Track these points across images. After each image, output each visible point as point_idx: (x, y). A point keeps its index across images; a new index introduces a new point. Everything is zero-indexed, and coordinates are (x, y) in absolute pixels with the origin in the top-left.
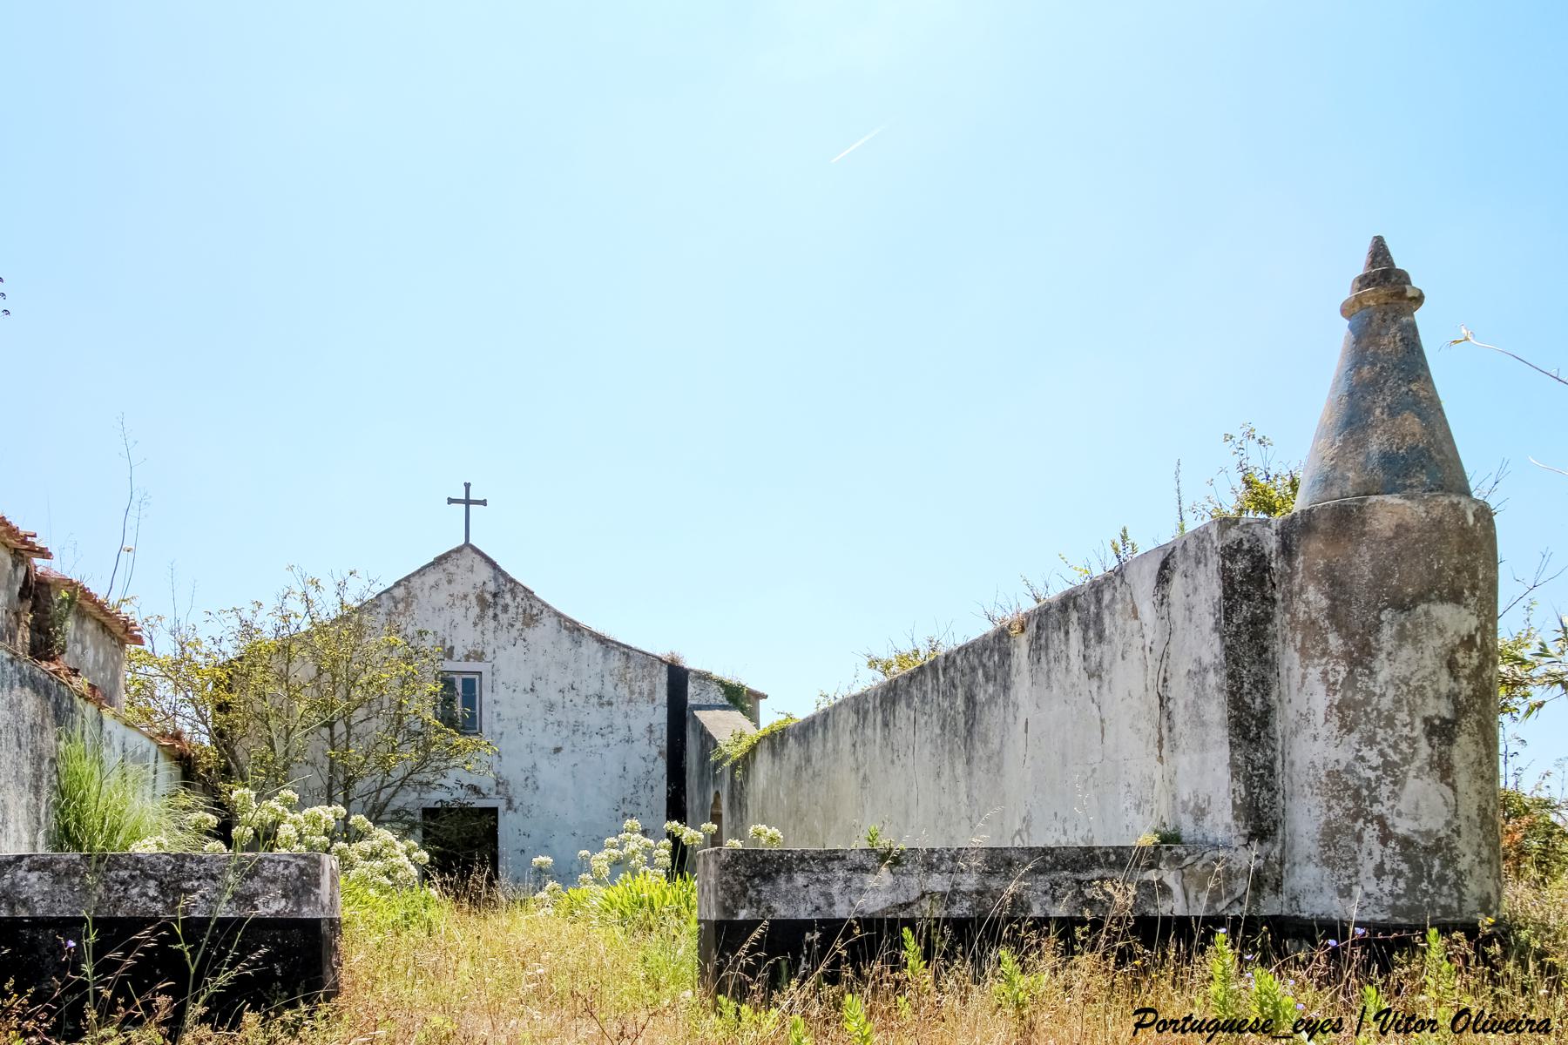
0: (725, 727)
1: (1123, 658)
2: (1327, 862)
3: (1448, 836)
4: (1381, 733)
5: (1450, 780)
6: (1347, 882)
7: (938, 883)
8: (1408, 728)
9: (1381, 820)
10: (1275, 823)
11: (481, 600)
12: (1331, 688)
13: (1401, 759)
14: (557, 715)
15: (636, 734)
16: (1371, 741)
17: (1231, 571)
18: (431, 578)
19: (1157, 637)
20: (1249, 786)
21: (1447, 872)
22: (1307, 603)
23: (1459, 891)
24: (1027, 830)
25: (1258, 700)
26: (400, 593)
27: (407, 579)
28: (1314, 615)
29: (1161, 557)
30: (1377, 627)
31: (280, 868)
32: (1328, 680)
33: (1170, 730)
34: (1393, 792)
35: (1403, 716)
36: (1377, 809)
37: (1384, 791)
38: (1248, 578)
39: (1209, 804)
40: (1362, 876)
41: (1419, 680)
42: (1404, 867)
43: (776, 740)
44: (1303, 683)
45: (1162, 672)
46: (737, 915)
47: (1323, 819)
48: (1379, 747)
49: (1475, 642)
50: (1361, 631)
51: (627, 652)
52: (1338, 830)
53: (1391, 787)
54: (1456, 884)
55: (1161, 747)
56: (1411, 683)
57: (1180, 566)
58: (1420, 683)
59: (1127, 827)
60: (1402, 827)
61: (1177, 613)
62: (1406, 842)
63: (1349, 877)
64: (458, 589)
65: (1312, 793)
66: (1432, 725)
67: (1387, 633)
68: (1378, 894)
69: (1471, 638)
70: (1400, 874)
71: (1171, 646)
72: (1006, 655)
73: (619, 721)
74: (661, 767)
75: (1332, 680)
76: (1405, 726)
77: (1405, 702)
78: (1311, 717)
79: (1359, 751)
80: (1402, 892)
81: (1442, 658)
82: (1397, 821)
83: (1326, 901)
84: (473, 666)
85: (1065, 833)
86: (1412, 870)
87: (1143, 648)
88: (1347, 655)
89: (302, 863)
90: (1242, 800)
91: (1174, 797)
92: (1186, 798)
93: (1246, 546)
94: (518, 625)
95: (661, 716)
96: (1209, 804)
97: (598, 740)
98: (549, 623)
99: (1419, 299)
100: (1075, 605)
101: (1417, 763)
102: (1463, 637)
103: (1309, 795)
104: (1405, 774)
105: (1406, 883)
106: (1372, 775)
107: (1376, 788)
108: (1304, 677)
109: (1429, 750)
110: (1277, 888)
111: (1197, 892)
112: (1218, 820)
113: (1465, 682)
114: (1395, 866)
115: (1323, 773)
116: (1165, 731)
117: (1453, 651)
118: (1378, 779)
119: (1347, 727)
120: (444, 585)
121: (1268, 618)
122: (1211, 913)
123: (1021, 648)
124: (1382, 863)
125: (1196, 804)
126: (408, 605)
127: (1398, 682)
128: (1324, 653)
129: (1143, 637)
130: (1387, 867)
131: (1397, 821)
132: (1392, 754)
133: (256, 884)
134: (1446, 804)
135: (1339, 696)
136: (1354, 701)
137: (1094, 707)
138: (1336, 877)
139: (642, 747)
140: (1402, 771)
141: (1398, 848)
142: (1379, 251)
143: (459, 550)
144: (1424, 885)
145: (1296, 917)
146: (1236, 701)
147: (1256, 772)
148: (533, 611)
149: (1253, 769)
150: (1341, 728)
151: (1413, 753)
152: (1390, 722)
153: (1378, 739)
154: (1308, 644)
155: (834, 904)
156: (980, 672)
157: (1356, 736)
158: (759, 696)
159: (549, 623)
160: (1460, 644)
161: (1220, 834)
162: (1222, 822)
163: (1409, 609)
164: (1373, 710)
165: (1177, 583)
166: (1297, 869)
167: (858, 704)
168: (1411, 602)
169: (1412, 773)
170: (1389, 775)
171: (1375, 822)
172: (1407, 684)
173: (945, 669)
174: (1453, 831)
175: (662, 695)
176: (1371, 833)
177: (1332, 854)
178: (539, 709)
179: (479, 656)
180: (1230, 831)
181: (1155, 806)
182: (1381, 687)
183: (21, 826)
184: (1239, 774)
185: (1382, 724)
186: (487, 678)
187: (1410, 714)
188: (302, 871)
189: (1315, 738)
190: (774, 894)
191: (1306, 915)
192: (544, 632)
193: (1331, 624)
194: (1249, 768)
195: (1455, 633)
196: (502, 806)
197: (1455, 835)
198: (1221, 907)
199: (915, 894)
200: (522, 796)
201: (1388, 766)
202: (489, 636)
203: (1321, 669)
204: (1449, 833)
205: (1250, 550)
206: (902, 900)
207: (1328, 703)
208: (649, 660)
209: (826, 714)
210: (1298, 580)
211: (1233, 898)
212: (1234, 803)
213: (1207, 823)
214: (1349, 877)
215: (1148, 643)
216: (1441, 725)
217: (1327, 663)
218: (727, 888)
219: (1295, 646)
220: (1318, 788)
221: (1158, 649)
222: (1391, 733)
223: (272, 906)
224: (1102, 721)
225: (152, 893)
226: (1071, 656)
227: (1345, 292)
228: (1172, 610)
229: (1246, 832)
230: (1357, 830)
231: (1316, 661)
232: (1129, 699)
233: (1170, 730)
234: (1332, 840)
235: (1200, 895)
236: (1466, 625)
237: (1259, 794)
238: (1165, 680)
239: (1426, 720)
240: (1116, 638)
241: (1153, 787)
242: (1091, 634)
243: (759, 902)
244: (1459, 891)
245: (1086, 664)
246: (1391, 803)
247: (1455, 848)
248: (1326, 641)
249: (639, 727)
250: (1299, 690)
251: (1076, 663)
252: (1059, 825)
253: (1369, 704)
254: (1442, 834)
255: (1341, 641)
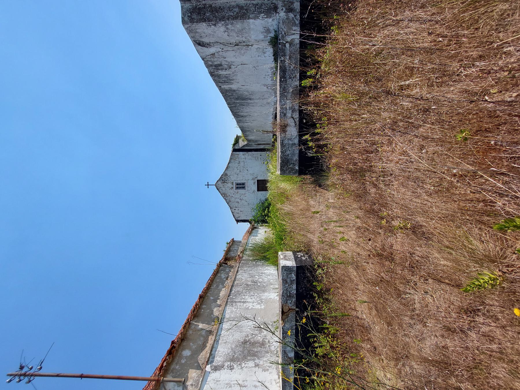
1: (225, 58)
7: (289, 115)
11: (224, 183)
17: (197, 20)
18: (221, 191)
24: (267, 85)
25: (235, 9)
26: (223, 195)
27: (221, 194)
29: (197, 45)
33: (244, 42)
38: (199, 13)
46: (297, 169)
51: (231, 159)
55: (249, 45)
57: (198, 38)
59: (269, 56)
64: (222, 186)
72: (227, 91)
73: (242, 160)
74: (250, 153)
84: (234, 184)
87: (222, 51)
89: (283, 270)
91: (263, 41)
92: (263, 36)
93: (189, 14)
94: (227, 177)
97: (245, 164)
98: (226, 172)
100: (213, 73)
111: (293, 30)
112: (270, 24)
116: (245, 44)
120: (222, 189)
121: (211, 6)
122: (299, 25)
123: (226, 87)
125: (265, 33)
126: (225, 194)
129: (219, 52)
133: (288, 280)
139: (246, 156)
143: (216, 186)
147: (257, 10)
148: (225, 174)
149: (256, 11)
155: (295, 143)
158: (237, 136)
159: (226, 172)
161: (275, 23)
165: (206, 40)
167: (238, 122)
173: (231, 105)
175: (238, 153)
178: (241, 173)
179: (233, 183)
180: (274, 19)
181: (264, 47)
183: (265, 269)
186: (236, 182)
188: (285, 270)
190: (292, 159)
192: (228, 173)
194: (255, 12)
196: (257, 179)
200: (255, 176)
202: (229, 181)
205: (190, 13)
208: (232, 154)
209: (240, 128)
211: (294, 18)
212: (266, 18)
213: (271, 28)
215: (221, 50)
218: (290, 172)
223: (294, 276)
224: (242, 64)
228: (212, 42)
229: (275, 14)
232: (236, 56)
233: (244, 42)
235: (294, 29)
237: (263, 9)
238: (230, 44)
241: (260, 48)
245: (228, 69)
249: (243, 157)
252: (266, 77)
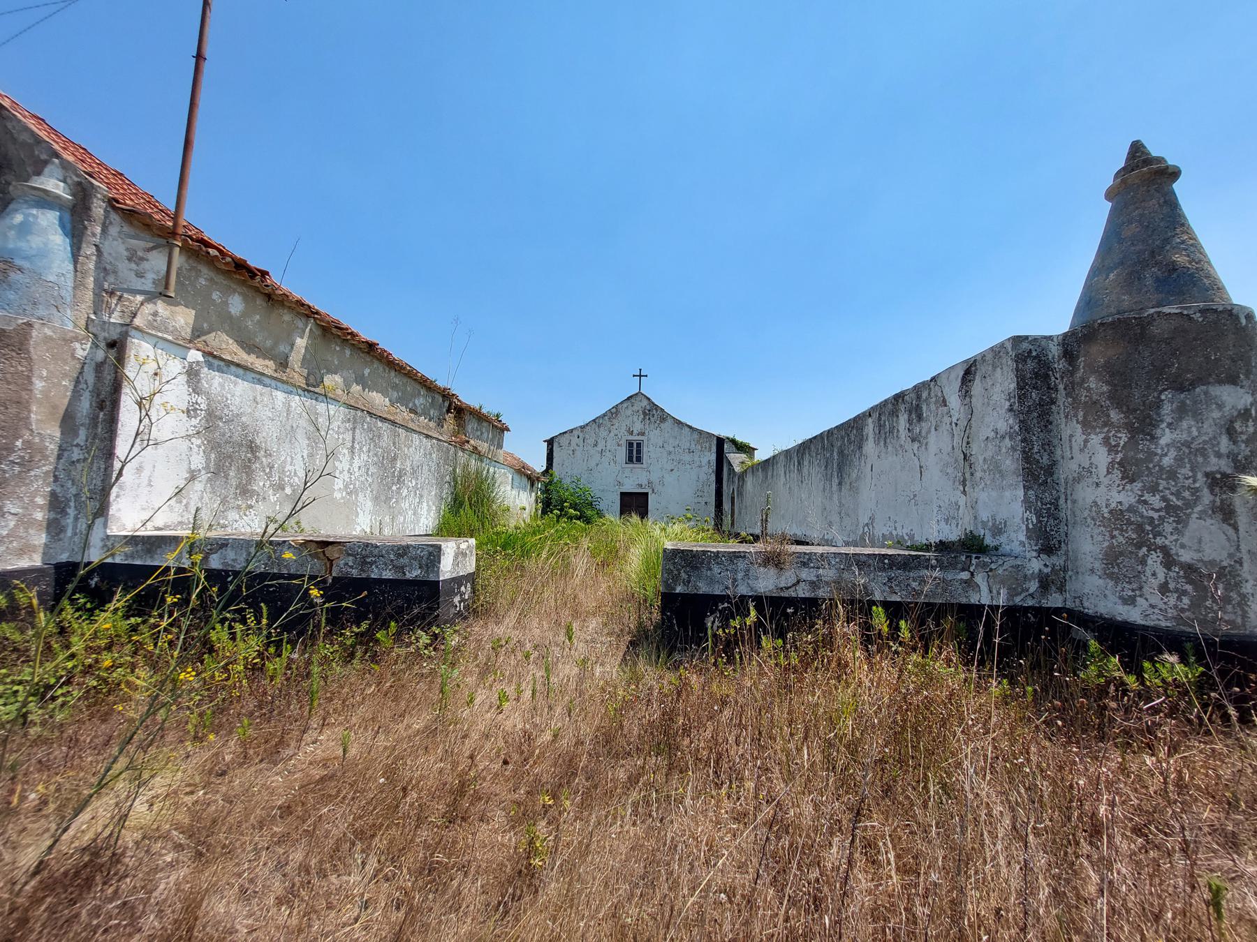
0: (736, 459)
1: (936, 430)
2: (1111, 576)
3: (1231, 565)
4: (1163, 484)
5: (1232, 522)
6: (1130, 593)
7: (805, 574)
8: (1191, 481)
9: (1165, 550)
10: (1060, 542)
11: (644, 413)
12: (1112, 449)
13: (1183, 504)
14: (672, 456)
15: (703, 464)
16: (1154, 489)
18: (625, 405)
19: (962, 416)
20: (1039, 515)
21: (1231, 594)
22: (1088, 389)
23: (1243, 610)
26: (614, 410)
28: (1095, 397)
29: (965, 367)
30: (1158, 404)
31: (418, 552)
32: (1110, 444)
33: (972, 474)
34: (1176, 529)
35: (1186, 471)
36: (1159, 541)
37: (1168, 528)
39: (1005, 526)
40: (1146, 589)
41: (1199, 444)
42: (1189, 588)
43: (755, 468)
44: (1085, 446)
45: (965, 438)
47: (1106, 544)
48: (1161, 494)
49: (1251, 414)
50: (1142, 408)
52: (1121, 554)
53: (1174, 525)
54: (1239, 604)
56: (1192, 446)
57: (982, 369)
58: (1201, 446)
60: (1186, 556)
61: (977, 402)
62: (1189, 569)
63: (1133, 590)
64: (635, 408)
65: (1095, 524)
66: (1214, 478)
67: (1167, 409)
68: (1164, 607)
69: (1247, 411)
70: (1185, 593)
71: (972, 422)
74: (713, 477)
75: (1113, 443)
76: (1187, 479)
77: (1186, 460)
78: (1094, 470)
79: (1142, 496)
80: (1186, 607)
81: (1221, 427)
82: (1181, 552)
83: (1110, 605)
85: (896, 529)
86: (1195, 589)
87: (951, 424)
88: (1129, 427)
90: (1033, 525)
91: (975, 517)
92: (985, 519)
94: (658, 422)
95: (713, 457)
96: (1005, 526)
97: (688, 466)
98: (670, 421)
99: (1175, 174)
101: (1199, 508)
102: (1240, 411)
103: (1092, 526)
104: (1188, 516)
105: (1191, 601)
106: (1156, 515)
107: (1159, 525)
108: (1086, 441)
109: (1212, 498)
110: (1061, 589)
113: (1243, 445)
114: (1179, 586)
115: (1106, 510)
116: (968, 476)
117: (1232, 422)
118: (1161, 519)
119: (1129, 478)
120: (630, 407)
122: (1011, 603)
123: (870, 427)
124: (1166, 583)
125: (994, 524)
126: (617, 415)
127: (1179, 445)
128: (1105, 424)
130: (1172, 586)
131: (1181, 552)
132: (1175, 500)
134: (1229, 539)
135: (1120, 456)
136: (1137, 459)
137: (916, 460)
138: (1119, 588)
139: (705, 469)
140: (1185, 514)
141: (1182, 573)
142: (1137, 149)
143: (637, 394)
144: (1208, 603)
145: (1080, 612)
146: (1027, 457)
148: (664, 417)
149: (1042, 504)
150: (1123, 478)
151: (1196, 500)
152: (1172, 475)
153: (1161, 488)
154: (1090, 418)
156: (846, 439)
157: (1138, 485)
158: (754, 449)
159: (670, 421)
160: (1237, 416)
161: (1017, 549)
162: (1016, 539)
163: (1189, 390)
164: (1154, 466)
166: (1080, 577)
167: (787, 453)
168: (1190, 385)
169: (1195, 516)
170: (1172, 516)
171: (1158, 550)
172: (1189, 447)
174: (1235, 561)
175: (714, 449)
176: (1154, 562)
177: (1116, 570)
178: (665, 454)
179: (643, 434)
182: (1162, 448)
184: (1031, 508)
185: (1164, 477)
187: (1192, 470)
188: (430, 554)
189: (1097, 485)
191: (1090, 612)
192: (668, 425)
193: (1112, 403)
195: (1233, 407)
196: (650, 492)
197: (1238, 565)
198: (1018, 600)
199: (793, 580)
200: (658, 488)
201: (1170, 509)
202: (647, 426)
203: (1103, 435)
204: (1232, 563)
205: (1037, 357)
206: (783, 585)
207: (1110, 460)
210: (1079, 374)
211: (1027, 593)
213: (1003, 539)
214: (1133, 590)
216: (1222, 478)
217: (1109, 431)
218: (669, 572)
219: (1077, 420)
220: (1101, 521)
221: (963, 423)
222: (1173, 483)
223: (414, 573)
224: (921, 467)
225: (350, 564)
226: (900, 429)
227: (1109, 182)
228: (974, 400)
229: (1037, 548)
230: (1140, 555)
231: (1098, 430)
233: (972, 474)
234: (1116, 561)
236: (1243, 401)
239: (1207, 475)
240: (932, 419)
241: (958, 509)
242: (914, 416)
243: (689, 582)
244: (1243, 610)
246: (1175, 537)
247: (1238, 575)
248: (1109, 416)
249: (705, 461)
250: (1081, 450)
251: (903, 433)
253: (1151, 461)
254: (1225, 564)
255: (1122, 416)
